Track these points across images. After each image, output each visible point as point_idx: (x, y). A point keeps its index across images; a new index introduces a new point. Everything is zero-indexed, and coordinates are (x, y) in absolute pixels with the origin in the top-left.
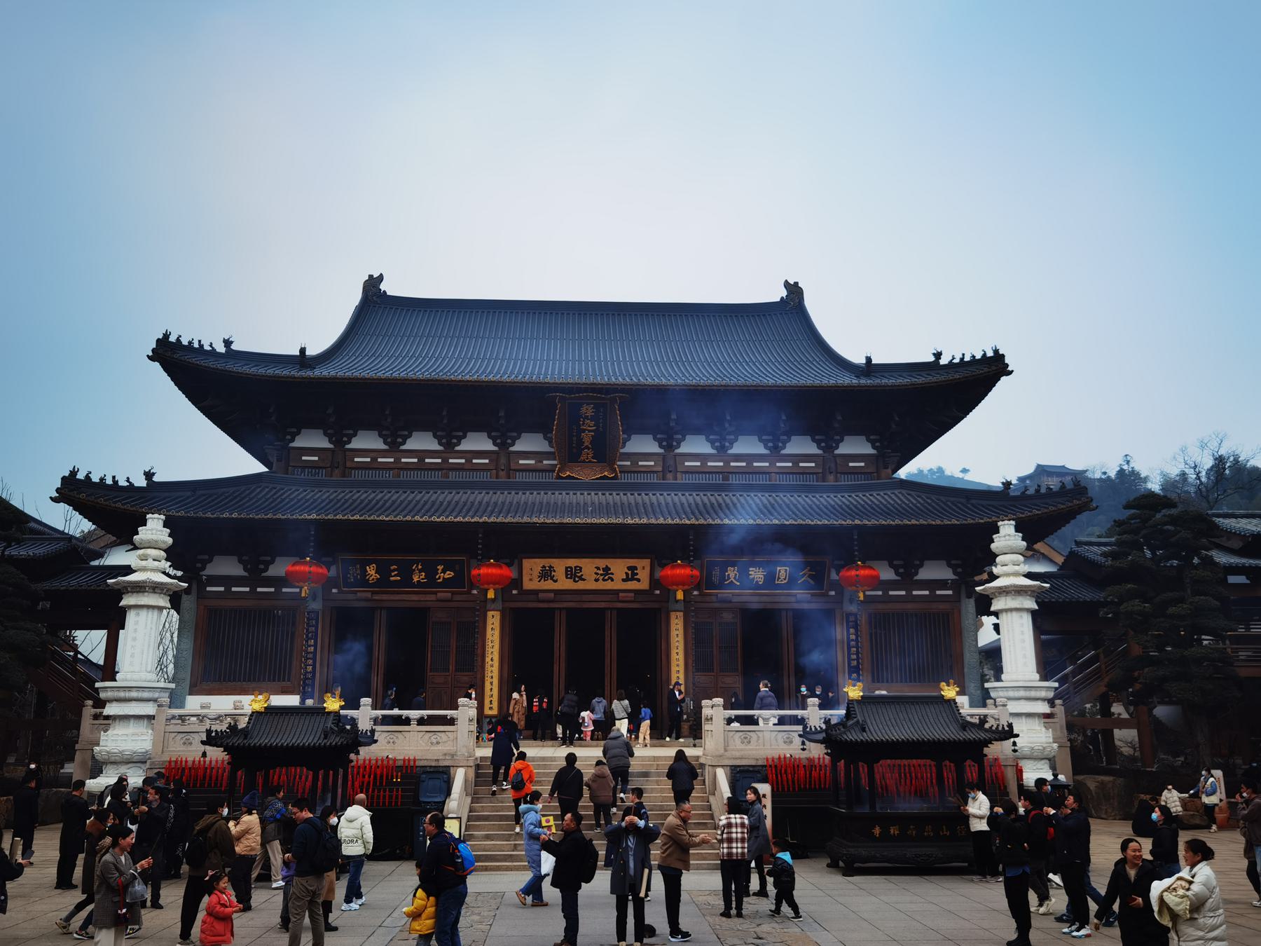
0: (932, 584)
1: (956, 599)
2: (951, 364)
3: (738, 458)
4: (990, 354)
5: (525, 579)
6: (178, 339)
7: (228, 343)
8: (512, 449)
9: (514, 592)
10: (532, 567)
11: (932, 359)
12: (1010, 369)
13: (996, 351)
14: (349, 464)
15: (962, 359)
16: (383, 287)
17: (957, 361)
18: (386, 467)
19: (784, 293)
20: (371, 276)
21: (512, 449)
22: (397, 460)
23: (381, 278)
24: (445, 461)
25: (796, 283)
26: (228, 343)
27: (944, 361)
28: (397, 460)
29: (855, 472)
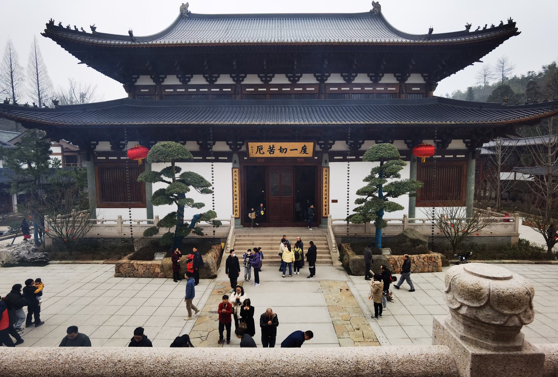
0: (456, 152)
1: (466, 161)
2: (477, 32)
3: (358, 85)
4: (506, 23)
5: (250, 151)
6: (60, 24)
7: (93, 28)
8: (242, 83)
9: (245, 158)
10: (253, 146)
11: (465, 29)
12: (518, 31)
13: (510, 21)
14: (318, 88)
15: (484, 28)
16: (189, 9)
17: (481, 29)
18: (181, 94)
19: (371, 8)
20: (183, 4)
21: (242, 83)
22: (351, 89)
23: (187, 5)
24: (374, 89)
25: (378, 2)
26: (93, 28)
27: (472, 30)
28: (351, 89)
29: (416, 92)
